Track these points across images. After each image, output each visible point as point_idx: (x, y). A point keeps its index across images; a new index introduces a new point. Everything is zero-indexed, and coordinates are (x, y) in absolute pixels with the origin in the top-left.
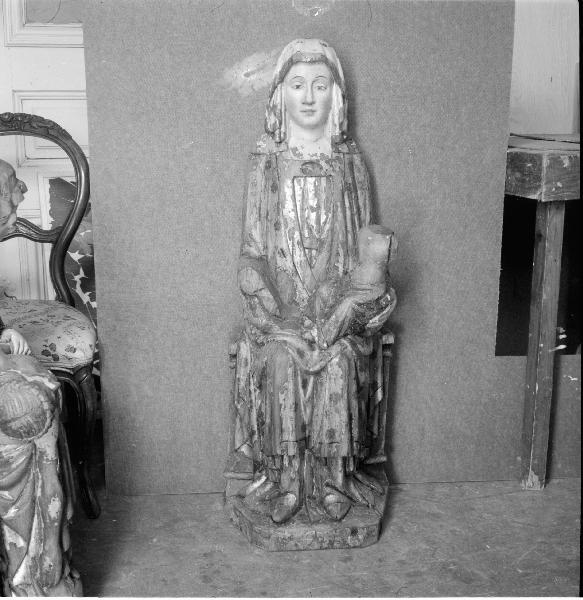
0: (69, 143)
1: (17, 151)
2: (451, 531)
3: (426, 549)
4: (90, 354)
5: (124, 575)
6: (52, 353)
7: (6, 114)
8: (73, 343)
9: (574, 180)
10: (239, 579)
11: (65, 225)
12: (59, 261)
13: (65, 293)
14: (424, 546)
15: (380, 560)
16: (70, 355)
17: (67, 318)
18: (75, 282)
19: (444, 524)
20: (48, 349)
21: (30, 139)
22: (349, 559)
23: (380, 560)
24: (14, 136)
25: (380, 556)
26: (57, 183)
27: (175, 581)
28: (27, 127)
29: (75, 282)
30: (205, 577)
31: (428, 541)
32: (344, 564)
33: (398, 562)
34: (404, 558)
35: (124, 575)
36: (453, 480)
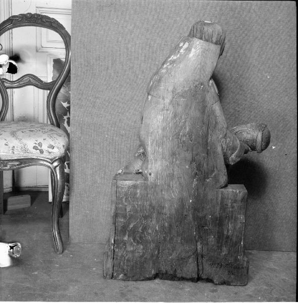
0: (63, 32)
1: (36, 44)
2: (282, 280)
3: (266, 289)
4: (62, 151)
5: (71, 287)
6: (39, 148)
7: (28, 13)
8: (52, 143)
9: (295, 140)
10: (144, 296)
11: (57, 80)
12: (52, 103)
13: (54, 121)
14: (265, 287)
15: (236, 293)
16: (50, 150)
17: (52, 130)
18: (64, 120)
19: (278, 275)
20: (37, 145)
21: (44, 30)
22: (216, 291)
23: (236, 293)
24: (35, 27)
25: (236, 291)
26: (57, 62)
27: (103, 294)
28: (40, 21)
29: (64, 120)
30: (122, 293)
31: (267, 285)
32: (212, 293)
33: (247, 295)
34: (251, 293)
35: (71, 287)
36: (284, 250)
